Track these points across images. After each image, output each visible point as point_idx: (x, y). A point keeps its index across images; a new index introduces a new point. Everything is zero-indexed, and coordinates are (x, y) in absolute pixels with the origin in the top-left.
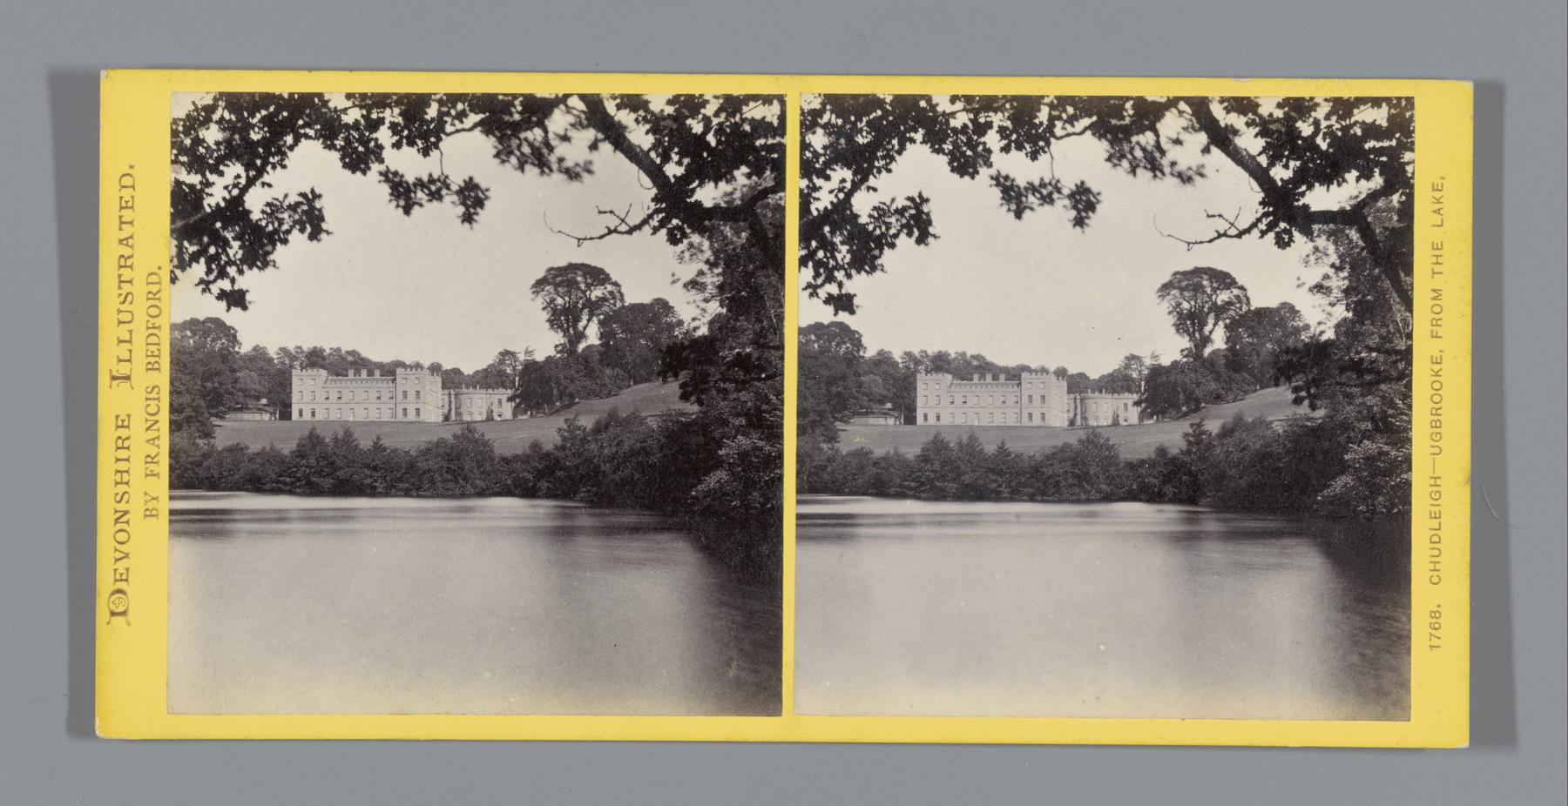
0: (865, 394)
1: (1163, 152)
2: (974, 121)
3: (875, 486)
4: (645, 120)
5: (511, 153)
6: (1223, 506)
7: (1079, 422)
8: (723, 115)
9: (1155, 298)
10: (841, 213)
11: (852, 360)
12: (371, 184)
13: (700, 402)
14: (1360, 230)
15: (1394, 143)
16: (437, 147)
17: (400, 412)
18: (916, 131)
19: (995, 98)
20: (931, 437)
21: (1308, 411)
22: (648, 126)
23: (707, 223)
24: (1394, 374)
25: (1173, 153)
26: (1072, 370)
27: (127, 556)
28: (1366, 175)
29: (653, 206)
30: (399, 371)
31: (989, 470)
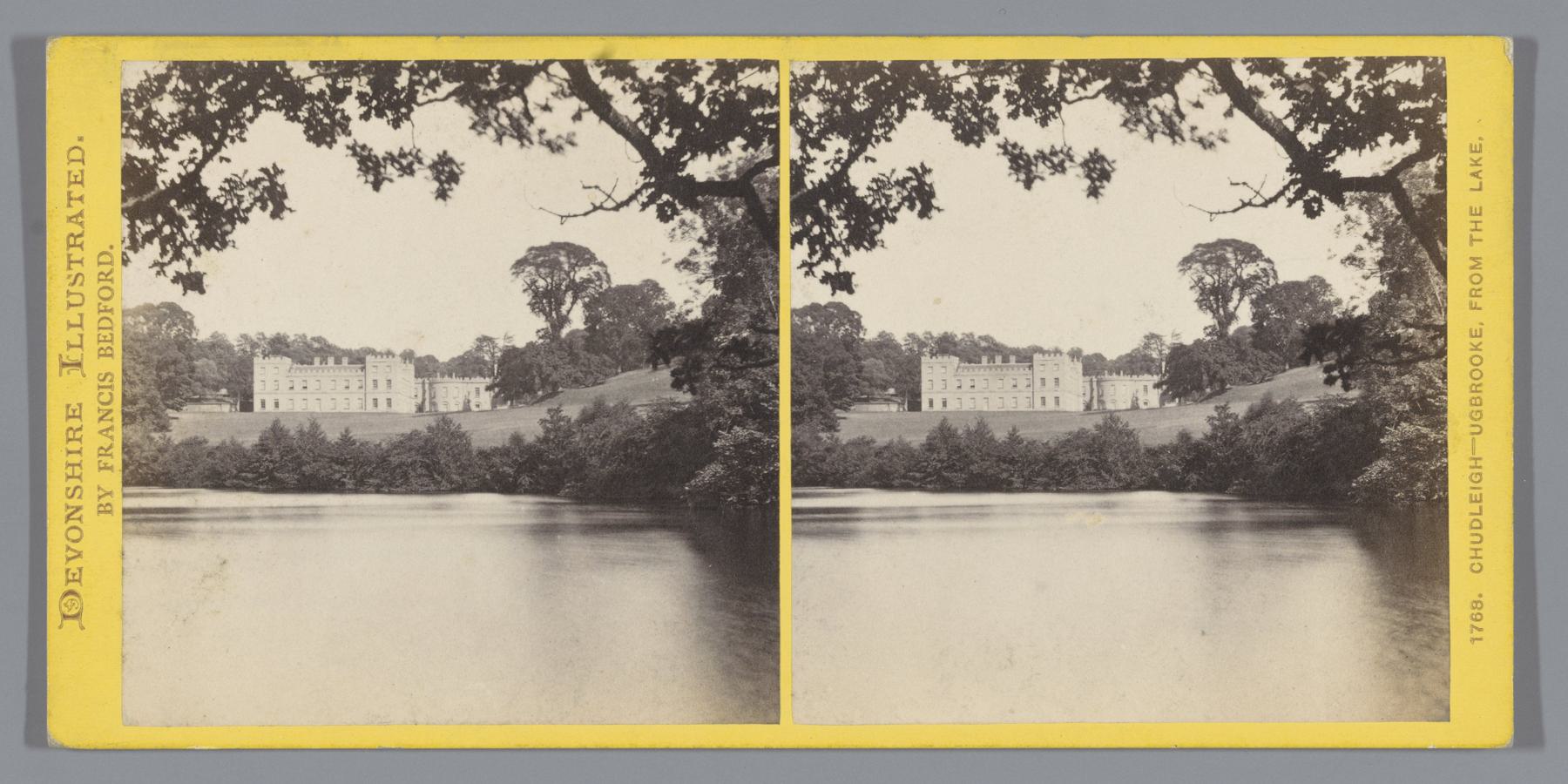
0: (199, 380)
1: (1182, 117)
2: (979, 85)
3: (876, 477)
4: (634, 89)
5: (488, 124)
6: (1248, 496)
7: (1095, 406)
8: (717, 83)
9: (509, 273)
10: (837, 187)
11: (850, 343)
12: (338, 158)
13: (693, 391)
14: (1396, 198)
15: (1430, 104)
16: (408, 119)
17: (1038, 403)
18: (917, 97)
19: (1002, 62)
20: (937, 424)
21: (1341, 391)
22: (636, 95)
23: (699, 198)
24: (1433, 350)
25: (1193, 117)
26: (1088, 351)
27: (79, 555)
28: (1401, 138)
29: (641, 181)
30: (1037, 357)
31: (332, 460)
